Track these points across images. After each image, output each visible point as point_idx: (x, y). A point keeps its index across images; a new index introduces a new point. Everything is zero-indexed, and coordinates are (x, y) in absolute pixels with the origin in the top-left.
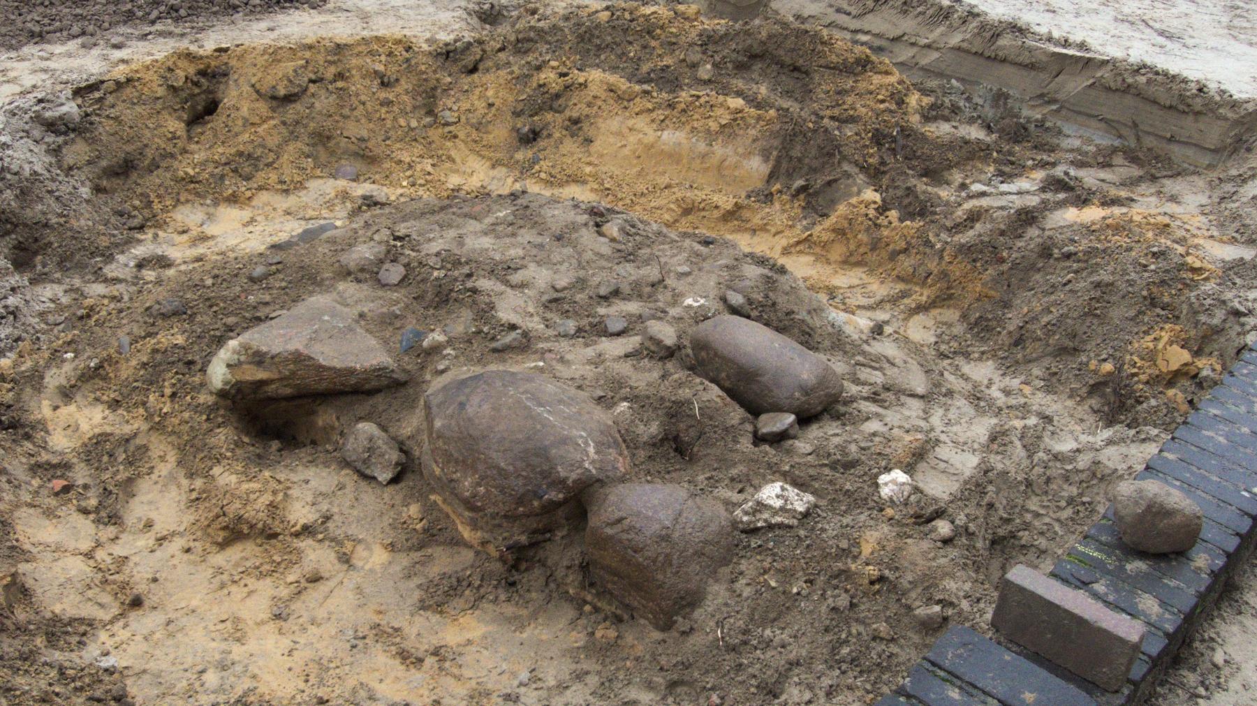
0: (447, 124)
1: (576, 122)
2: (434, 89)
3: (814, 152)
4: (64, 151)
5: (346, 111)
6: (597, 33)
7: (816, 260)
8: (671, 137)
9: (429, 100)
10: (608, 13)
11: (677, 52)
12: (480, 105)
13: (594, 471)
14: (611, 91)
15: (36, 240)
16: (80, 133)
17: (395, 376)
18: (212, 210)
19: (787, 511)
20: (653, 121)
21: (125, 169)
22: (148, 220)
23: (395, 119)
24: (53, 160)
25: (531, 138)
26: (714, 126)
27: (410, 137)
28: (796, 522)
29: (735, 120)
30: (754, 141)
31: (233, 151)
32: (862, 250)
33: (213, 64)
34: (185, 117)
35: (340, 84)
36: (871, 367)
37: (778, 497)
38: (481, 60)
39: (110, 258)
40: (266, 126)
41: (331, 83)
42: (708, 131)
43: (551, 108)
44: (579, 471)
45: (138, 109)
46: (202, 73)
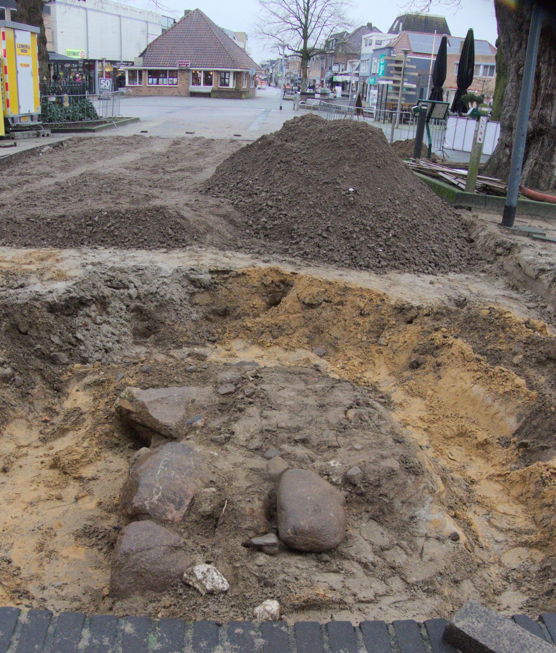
0: (380, 345)
1: (439, 365)
2: (385, 325)
3: (547, 426)
4: (196, 296)
5: (335, 321)
6: (474, 320)
7: (503, 490)
8: (479, 390)
9: (380, 328)
10: (488, 311)
11: (511, 344)
12: (401, 340)
13: (148, 508)
14: (462, 353)
15: (156, 328)
16: (208, 290)
17: (171, 433)
18: (248, 346)
19: (202, 584)
20: (473, 377)
21: (225, 313)
22: (219, 340)
23: (357, 333)
24: (188, 297)
25: (415, 365)
26: (501, 391)
27: (359, 345)
28: (204, 593)
29: (513, 391)
30: (518, 407)
31: (274, 322)
32: (528, 495)
33: (288, 279)
34: (268, 300)
35: (339, 307)
36: (406, 551)
37: (203, 573)
38: (416, 317)
39: (180, 347)
40: (294, 316)
41: (335, 304)
42: (497, 393)
43: (432, 354)
44: (140, 503)
45: (243, 289)
46: (283, 282)
